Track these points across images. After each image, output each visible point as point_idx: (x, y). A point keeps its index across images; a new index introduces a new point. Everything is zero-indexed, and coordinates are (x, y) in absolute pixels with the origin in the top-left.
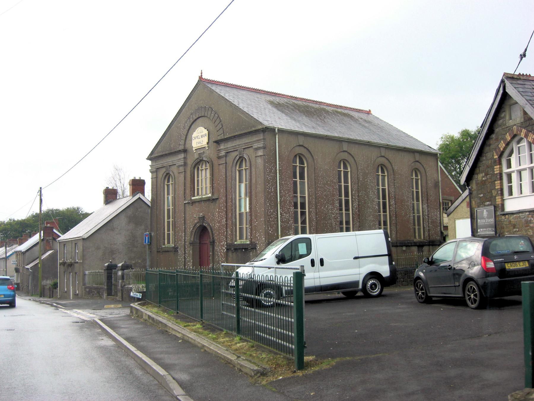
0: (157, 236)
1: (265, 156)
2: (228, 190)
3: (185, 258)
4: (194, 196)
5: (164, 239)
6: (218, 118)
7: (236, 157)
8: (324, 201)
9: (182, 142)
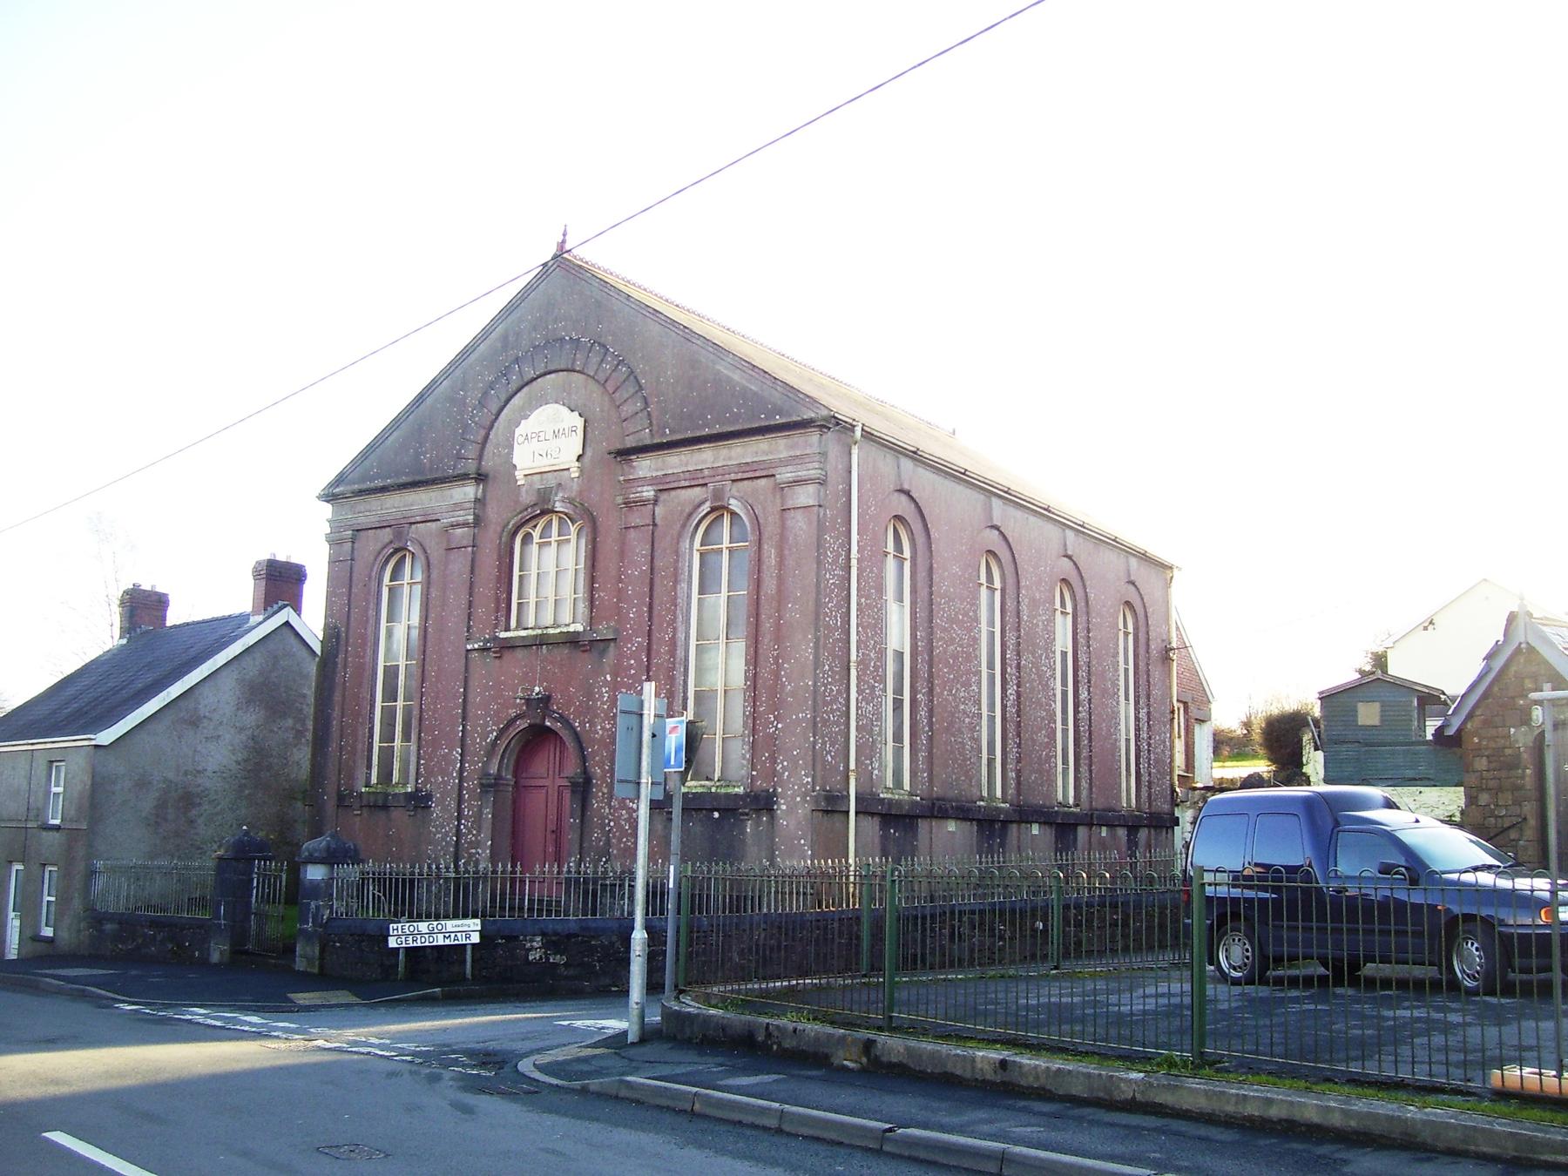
0: (341, 755)
1: (822, 510)
2: (655, 613)
3: (458, 833)
4: (507, 629)
5: (369, 767)
6: (632, 377)
7: (699, 505)
8: (949, 673)
9: (471, 451)
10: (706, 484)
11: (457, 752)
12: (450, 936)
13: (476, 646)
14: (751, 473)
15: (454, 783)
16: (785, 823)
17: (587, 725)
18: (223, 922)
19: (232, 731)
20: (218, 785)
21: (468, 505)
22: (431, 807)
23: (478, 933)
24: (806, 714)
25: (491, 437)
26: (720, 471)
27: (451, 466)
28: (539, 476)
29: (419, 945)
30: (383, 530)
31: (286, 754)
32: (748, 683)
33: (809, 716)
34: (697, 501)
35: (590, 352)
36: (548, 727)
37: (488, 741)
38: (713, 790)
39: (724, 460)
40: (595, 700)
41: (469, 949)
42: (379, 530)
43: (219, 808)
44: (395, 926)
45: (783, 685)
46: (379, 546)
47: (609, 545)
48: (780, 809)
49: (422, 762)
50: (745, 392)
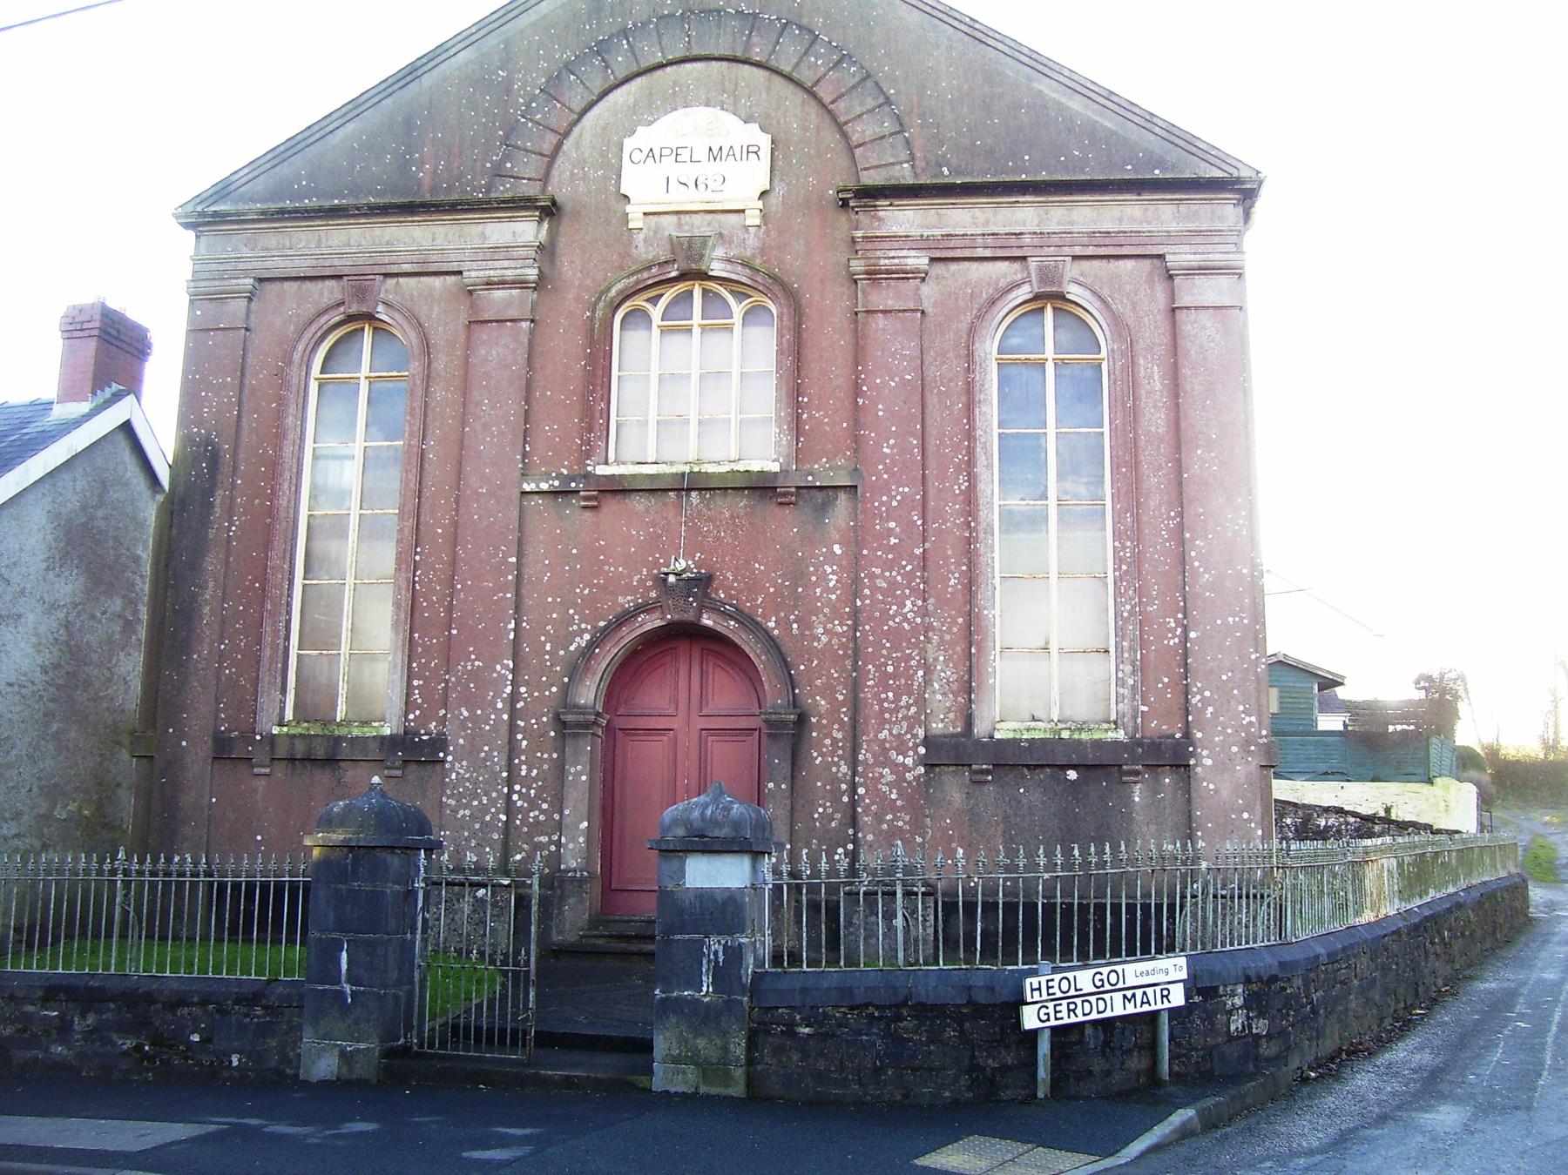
3: (509, 808)
5: (284, 691)
9: (529, 167)
10: (1024, 258)
11: (505, 667)
12: (1134, 995)
13: (544, 486)
14: (1107, 249)
15: (499, 719)
16: (1212, 786)
17: (795, 626)
18: (348, 988)
19: (39, 608)
20: (13, 709)
21: (522, 253)
22: (443, 761)
23: (1182, 984)
24: (1242, 619)
25: (565, 147)
26: (1055, 240)
27: (482, 186)
28: (674, 218)
29: (1081, 1018)
30: (320, 284)
31: (110, 662)
32: (1124, 567)
33: (1246, 621)
34: (1003, 283)
35: (781, 35)
36: (706, 628)
37: (572, 648)
38: (1065, 735)
39: (1058, 224)
40: (811, 586)
41: (1165, 1017)
42: (308, 285)
43: (14, 752)
44: (1034, 981)
45: (1195, 571)
46: (310, 310)
47: (830, 336)
48: (1203, 765)
49: (415, 683)
50: (1092, 130)
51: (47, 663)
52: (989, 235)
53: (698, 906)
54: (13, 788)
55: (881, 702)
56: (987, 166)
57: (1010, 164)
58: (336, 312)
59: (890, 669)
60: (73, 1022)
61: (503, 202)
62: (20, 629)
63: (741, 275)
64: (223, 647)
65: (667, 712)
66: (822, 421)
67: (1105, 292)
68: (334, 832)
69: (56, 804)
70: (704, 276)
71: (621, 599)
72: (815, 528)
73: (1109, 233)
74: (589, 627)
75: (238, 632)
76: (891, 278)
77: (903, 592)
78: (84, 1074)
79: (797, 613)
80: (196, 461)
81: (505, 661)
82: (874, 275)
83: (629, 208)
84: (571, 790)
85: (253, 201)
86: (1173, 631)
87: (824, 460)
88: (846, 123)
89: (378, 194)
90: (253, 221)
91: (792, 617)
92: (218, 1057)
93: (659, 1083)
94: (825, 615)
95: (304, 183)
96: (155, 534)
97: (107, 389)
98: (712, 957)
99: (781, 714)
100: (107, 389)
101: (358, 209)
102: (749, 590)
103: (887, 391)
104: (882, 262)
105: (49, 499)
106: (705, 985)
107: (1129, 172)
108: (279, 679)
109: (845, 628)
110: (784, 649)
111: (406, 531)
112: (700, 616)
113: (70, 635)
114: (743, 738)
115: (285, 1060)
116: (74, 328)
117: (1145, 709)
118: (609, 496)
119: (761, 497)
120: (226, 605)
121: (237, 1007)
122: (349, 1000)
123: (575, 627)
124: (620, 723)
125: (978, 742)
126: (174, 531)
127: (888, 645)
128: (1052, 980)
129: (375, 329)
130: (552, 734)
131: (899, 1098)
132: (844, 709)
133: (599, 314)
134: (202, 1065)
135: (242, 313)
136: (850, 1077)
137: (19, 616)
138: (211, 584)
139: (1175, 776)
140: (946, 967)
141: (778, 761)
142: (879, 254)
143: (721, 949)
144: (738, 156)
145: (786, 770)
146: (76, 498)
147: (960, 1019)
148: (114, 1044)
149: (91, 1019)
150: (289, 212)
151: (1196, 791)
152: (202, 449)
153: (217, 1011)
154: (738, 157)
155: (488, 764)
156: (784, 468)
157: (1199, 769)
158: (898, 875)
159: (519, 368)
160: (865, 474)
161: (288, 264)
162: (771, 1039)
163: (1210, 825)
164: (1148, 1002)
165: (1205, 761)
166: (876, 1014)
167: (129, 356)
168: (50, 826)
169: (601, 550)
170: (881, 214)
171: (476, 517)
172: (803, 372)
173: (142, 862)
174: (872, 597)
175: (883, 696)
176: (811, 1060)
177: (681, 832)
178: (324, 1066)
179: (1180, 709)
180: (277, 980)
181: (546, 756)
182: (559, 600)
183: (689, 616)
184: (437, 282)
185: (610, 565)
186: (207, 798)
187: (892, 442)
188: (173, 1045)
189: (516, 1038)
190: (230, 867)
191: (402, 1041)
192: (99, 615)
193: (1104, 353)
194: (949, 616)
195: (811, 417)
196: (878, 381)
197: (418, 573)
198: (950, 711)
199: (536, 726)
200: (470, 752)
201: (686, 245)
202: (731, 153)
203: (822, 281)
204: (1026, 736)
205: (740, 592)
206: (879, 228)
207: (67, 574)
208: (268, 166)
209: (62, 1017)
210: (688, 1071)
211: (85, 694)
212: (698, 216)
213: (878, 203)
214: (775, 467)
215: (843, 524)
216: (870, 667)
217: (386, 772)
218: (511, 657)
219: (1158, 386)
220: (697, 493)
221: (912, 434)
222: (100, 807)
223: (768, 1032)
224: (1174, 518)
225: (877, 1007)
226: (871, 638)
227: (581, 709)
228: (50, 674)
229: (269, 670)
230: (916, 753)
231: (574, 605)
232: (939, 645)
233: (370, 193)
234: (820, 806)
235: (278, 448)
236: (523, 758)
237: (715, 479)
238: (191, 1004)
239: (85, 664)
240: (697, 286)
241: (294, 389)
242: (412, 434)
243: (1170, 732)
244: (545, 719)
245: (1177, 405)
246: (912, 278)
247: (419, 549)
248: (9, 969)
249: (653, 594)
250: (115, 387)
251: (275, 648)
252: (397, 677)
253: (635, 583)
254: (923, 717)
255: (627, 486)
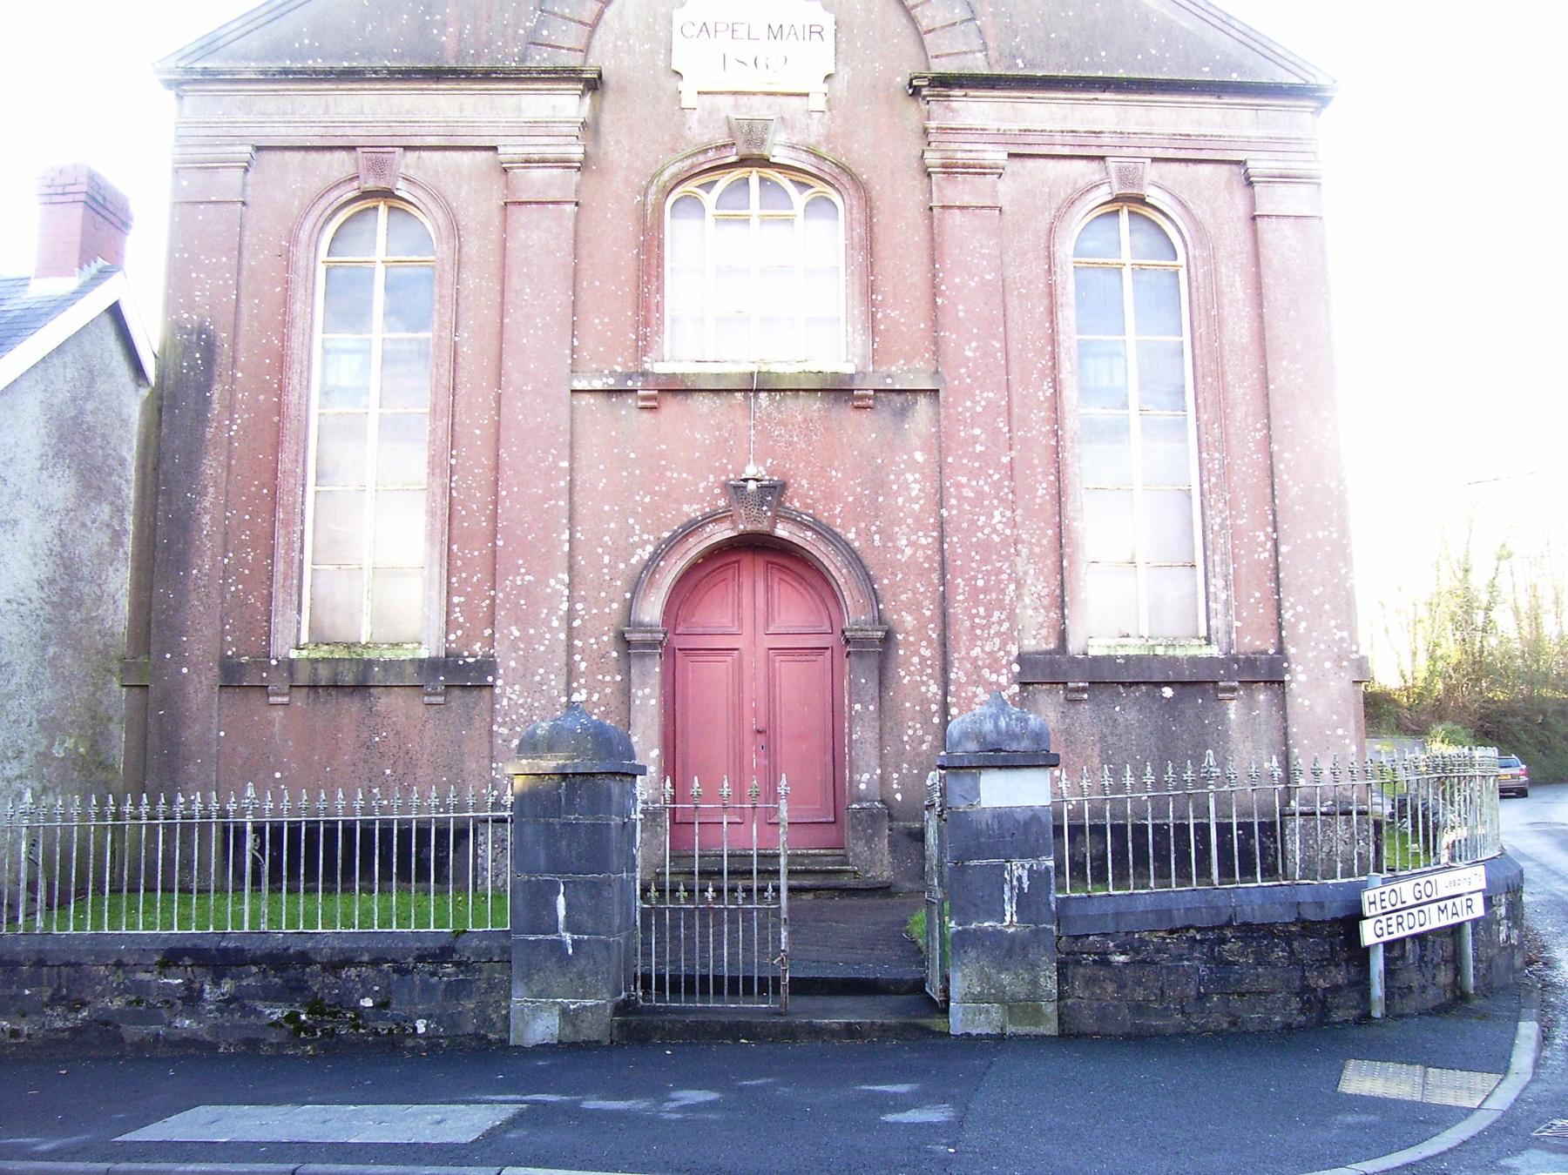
5: (300, 612)
10: (1102, 158)
11: (561, 582)
13: (598, 385)
16: (1307, 703)
18: (568, 937)
21: (565, 129)
24: (1331, 533)
26: (1135, 141)
28: (731, 99)
30: (328, 155)
31: (100, 578)
34: (1081, 183)
37: (634, 561)
38: (1160, 651)
42: (314, 155)
43: (14, 681)
46: (317, 184)
48: (1297, 681)
49: (456, 600)
51: (43, 577)
52: (1067, 132)
53: (996, 827)
54: (14, 722)
55: (972, 617)
56: (1063, 60)
57: (1087, 59)
58: (348, 187)
59: (980, 583)
60: (202, 991)
61: (544, 72)
62: (17, 536)
63: (806, 162)
64: (226, 561)
65: (732, 630)
66: (898, 321)
67: (1185, 196)
68: (541, 758)
69: (54, 742)
70: (764, 162)
71: (686, 508)
72: (894, 434)
73: (1188, 135)
74: (652, 538)
75: (244, 544)
76: (967, 173)
77: (991, 503)
78: (221, 1050)
79: (878, 523)
80: (187, 350)
81: (560, 576)
82: (949, 169)
83: (681, 86)
84: (639, 715)
85: (246, 58)
86: (1263, 545)
87: (902, 362)
88: (915, 6)
89: (394, 57)
90: (250, 81)
91: (874, 528)
92: (398, 1024)
93: (960, 1020)
94: (908, 526)
95: (307, 42)
96: (140, 433)
97: (93, 263)
98: (1015, 883)
99: (867, 631)
100: (93, 263)
101: (375, 72)
102: (826, 499)
103: (966, 291)
104: (959, 155)
105: (42, 387)
106: (1008, 914)
107: (1206, 74)
108: (295, 597)
109: (930, 540)
110: (865, 562)
111: (439, 431)
112: (774, 526)
113: (64, 545)
114: (813, 658)
115: (487, 1022)
116: (56, 194)
117: (1238, 624)
118: (669, 396)
119: (835, 400)
120: (228, 514)
121: (420, 965)
122: (570, 951)
123: (636, 538)
124: (679, 643)
125: (1073, 659)
126: (165, 430)
127: (977, 558)
128: (1384, 893)
129: (391, 208)
130: (615, 654)
131: (1225, 1026)
132: (932, 626)
133: (651, 198)
134: (377, 1033)
135: (238, 185)
136: (1172, 1006)
137: (16, 522)
138: (211, 490)
139: (1269, 692)
140: (1265, 884)
141: (867, 682)
142: (953, 146)
143: (1025, 875)
144: (800, 35)
145: (873, 688)
146: (66, 388)
147: (1289, 939)
148: (259, 1014)
149: (227, 986)
150: (294, 73)
151: (1292, 707)
152: (195, 337)
153: (394, 971)
154: (801, 37)
155: (544, 688)
156: (859, 369)
157: (1293, 685)
158: (1210, 787)
159: (563, 254)
160: (947, 378)
161: (292, 131)
162: (1081, 970)
163: (1306, 742)
164: (1457, 914)
165: (1298, 678)
166: (1198, 937)
167: (113, 229)
168: (49, 765)
169: (661, 454)
170: (954, 104)
171: (520, 417)
172: (876, 269)
173: (137, 804)
174: (959, 507)
175: (974, 611)
176: (1127, 991)
177: (972, 746)
178: (542, 1027)
179: (1272, 624)
180: (465, 932)
181: (608, 678)
182: (616, 508)
183: (764, 526)
184: (466, 157)
185: (671, 470)
186: (215, 732)
187: (974, 344)
188: (339, 1012)
189: (769, 986)
190: (231, 807)
191: (623, 995)
192: (89, 523)
193: (1181, 259)
194: (1038, 528)
195: (886, 316)
196: (957, 280)
197: (454, 478)
198: (1041, 626)
199: (595, 647)
200: (525, 673)
201: (746, 128)
202: (792, 32)
203: (892, 173)
204: (1121, 652)
205: (816, 501)
206: (953, 119)
207: (59, 474)
208: (263, 20)
209: (188, 985)
210: (991, 1009)
211: (78, 615)
212: (757, 98)
213: (951, 93)
214: (849, 369)
215: (924, 431)
216: (959, 580)
217: (426, 699)
218: (566, 570)
219: (1240, 295)
220: (766, 394)
221: (994, 337)
222: (94, 744)
223: (1078, 963)
224: (1261, 430)
225: (1199, 930)
226: (959, 550)
227: (649, 628)
228: (46, 590)
229: (283, 586)
230: (1010, 670)
231: (634, 513)
232: (1028, 558)
233: (385, 56)
234: (910, 727)
235: (284, 339)
236: (582, 681)
237: (787, 380)
238: (361, 964)
239: (78, 580)
240: (754, 173)
241: (302, 272)
242: (442, 326)
243: (1263, 647)
244: (605, 638)
245: (1261, 316)
246: (989, 174)
247: (454, 452)
248: (107, 931)
249: (722, 503)
250: (101, 263)
251: (289, 563)
252: (434, 593)
253: (701, 491)
254: (1016, 633)
255: (690, 385)
